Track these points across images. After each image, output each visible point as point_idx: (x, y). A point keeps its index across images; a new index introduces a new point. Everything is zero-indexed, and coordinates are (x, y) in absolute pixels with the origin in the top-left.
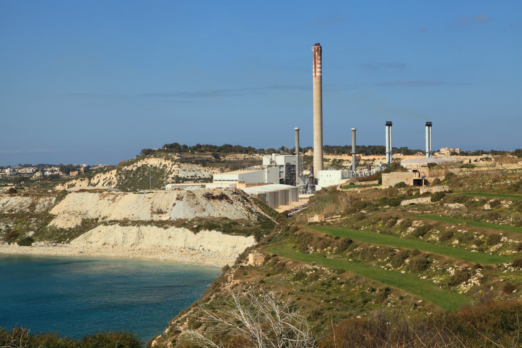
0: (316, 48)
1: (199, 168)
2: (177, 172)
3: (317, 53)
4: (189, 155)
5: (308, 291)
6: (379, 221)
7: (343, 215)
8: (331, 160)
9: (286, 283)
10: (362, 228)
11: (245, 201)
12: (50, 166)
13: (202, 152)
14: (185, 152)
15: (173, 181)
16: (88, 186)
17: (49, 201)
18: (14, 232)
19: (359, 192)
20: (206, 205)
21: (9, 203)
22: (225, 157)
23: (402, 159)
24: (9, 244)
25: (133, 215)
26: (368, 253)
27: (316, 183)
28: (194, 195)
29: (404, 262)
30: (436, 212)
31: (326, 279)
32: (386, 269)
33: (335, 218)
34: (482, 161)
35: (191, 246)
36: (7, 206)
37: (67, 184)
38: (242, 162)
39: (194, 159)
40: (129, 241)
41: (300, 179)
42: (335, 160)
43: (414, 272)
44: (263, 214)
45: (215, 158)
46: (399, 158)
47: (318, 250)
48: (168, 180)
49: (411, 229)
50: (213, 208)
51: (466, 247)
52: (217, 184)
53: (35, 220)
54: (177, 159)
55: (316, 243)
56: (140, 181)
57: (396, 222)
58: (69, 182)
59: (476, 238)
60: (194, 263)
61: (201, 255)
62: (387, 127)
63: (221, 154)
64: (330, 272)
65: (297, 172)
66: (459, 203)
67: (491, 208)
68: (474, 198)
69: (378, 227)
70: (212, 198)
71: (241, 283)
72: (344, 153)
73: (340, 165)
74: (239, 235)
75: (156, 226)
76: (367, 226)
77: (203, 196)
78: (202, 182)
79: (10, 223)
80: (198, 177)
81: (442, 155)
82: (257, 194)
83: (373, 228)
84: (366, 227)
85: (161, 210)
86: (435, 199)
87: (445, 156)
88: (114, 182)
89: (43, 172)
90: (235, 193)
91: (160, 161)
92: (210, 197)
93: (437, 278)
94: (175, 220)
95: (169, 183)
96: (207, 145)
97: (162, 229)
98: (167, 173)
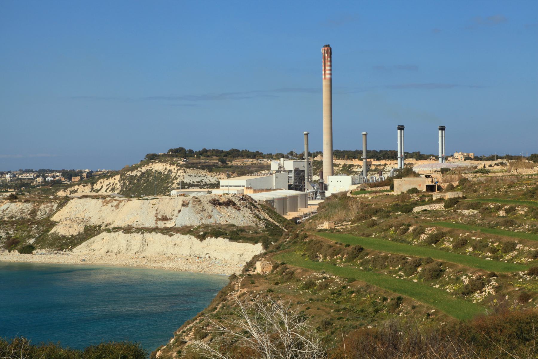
0: (326, 50)
1: (205, 173)
2: (182, 178)
3: (326, 55)
4: (195, 159)
5: (318, 300)
6: (391, 228)
7: (353, 222)
8: (341, 165)
9: (295, 292)
10: (373, 235)
11: (252, 207)
12: (52, 171)
13: (208, 156)
14: (191, 156)
15: (179, 186)
16: (91, 191)
17: (51, 208)
18: (14, 239)
19: (370, 198)
20: (212, 211)
21: (9, 209)
22: (231, 162)
23: (415, 164)
24: (10, 252)
25: (137, 222)
26: (380, 261)
27: (326, 189)
28: (200, 201)
29: (417, 271)
30: (450, 219)
31: (336, 287)
32: (398, 277)
33: (345, 225)
34: (497, 166)
35: (197, 253)
36: (7, 212)
37: (69, 189)
38: (249, 167)
39: (200, 164)
40: (133, 248)
41: (309, 185)
42: (345, 165)
43: (427, 281)
44: (271, 220)
45: (222, 163)
46: (411, 163)
47: (327, 258)
48: (173, 186)
49: (423, 237)
50: (220, 214)
51: (480, 255)
52: (224, 190)
53: (36, 227)
54: (182, 164)
55: (326, 250)
56: (144, 186)
57: (408, 229)
58: (71, 188)
59: (491, 245)
60: (200, 272)
61: (207, 263)
62: (399, 131)
63: (228, 159)
64: (340, 280)
65: (306, 178)
66: (473, 210)
67: (506, 215)
68: (488, 204)
69: (390, 234)
70: (218, 205)
71: (248, 292)
72: (354, 158)
73: (351, 170)
74: (247, 243)
75: (161, 233)
76: (379, 233)
77: (210, 202)
78: (208, 187)
79: (10, 230)
80: (204, 183)
81: (456, 160)
82: (264, 200)
83: (385, 235)
84: (377, 235)
85: (166, 216)
86: (448, 205)
87: (459, 161)
88: (117, 187)
89: (44, 177)
90: (242, 199)
91: (165, 167)
92: (217, 203)
93: (450, 287)
94: (181, 227)
95: (174, 189)
96: (214, 150)
97: (167, 236)
98: (172, 178)
